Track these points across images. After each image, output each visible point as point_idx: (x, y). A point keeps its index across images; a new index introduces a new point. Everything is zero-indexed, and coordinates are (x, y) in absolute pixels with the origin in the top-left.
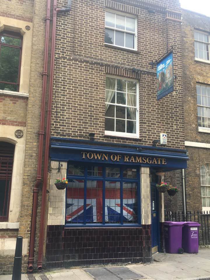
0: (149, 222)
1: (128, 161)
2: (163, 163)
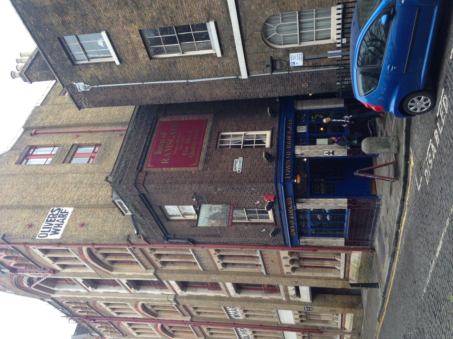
0: (346, 200)
2: (291, 199)
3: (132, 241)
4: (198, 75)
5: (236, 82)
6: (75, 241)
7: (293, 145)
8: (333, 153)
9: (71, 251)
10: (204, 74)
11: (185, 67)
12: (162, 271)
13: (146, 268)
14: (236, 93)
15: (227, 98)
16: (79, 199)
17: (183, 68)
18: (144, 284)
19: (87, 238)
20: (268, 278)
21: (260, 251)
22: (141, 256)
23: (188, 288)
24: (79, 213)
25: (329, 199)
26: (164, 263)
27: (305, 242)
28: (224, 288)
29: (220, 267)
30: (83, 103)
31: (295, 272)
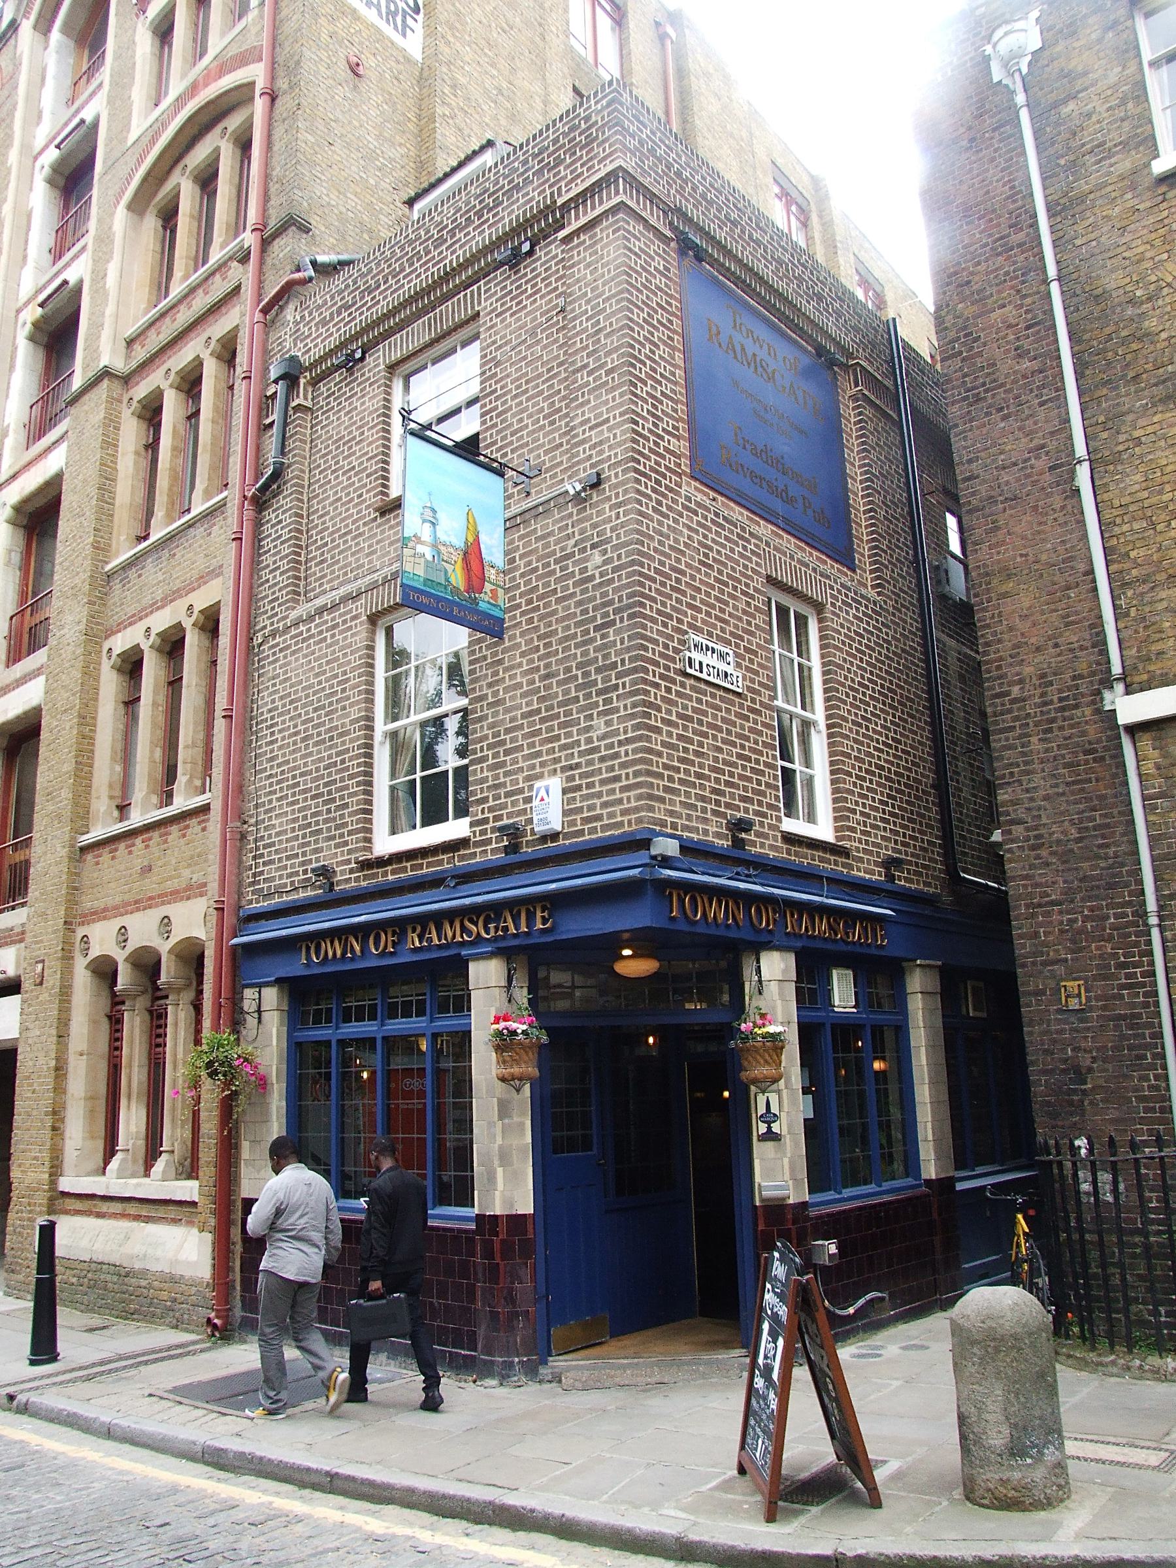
1: (417, 944)
3: (278, 243)
4: (1116, 503)
5: (1081, 677)
6: (288, 28)
7: (799, 944)
8: (770, 1136)
9: (240, 26)
10: (1125, 528)
11: (1162, 443)
12: (113, 401)
13: (130, 343)
15: (987, 644)
16: (454, 87)
17: (1153, 438)
18: (53, 364)
19: (305, 67)
20: (64, 852)
21: (205, 809)
22: (194, 307)
23: (20, 535)
24: (400, 73)
25: (528, 1123)
26: (151, 413)
27: (259, 1011)
28: (18, 675)
29: (120, 643)
31: (89, 973)
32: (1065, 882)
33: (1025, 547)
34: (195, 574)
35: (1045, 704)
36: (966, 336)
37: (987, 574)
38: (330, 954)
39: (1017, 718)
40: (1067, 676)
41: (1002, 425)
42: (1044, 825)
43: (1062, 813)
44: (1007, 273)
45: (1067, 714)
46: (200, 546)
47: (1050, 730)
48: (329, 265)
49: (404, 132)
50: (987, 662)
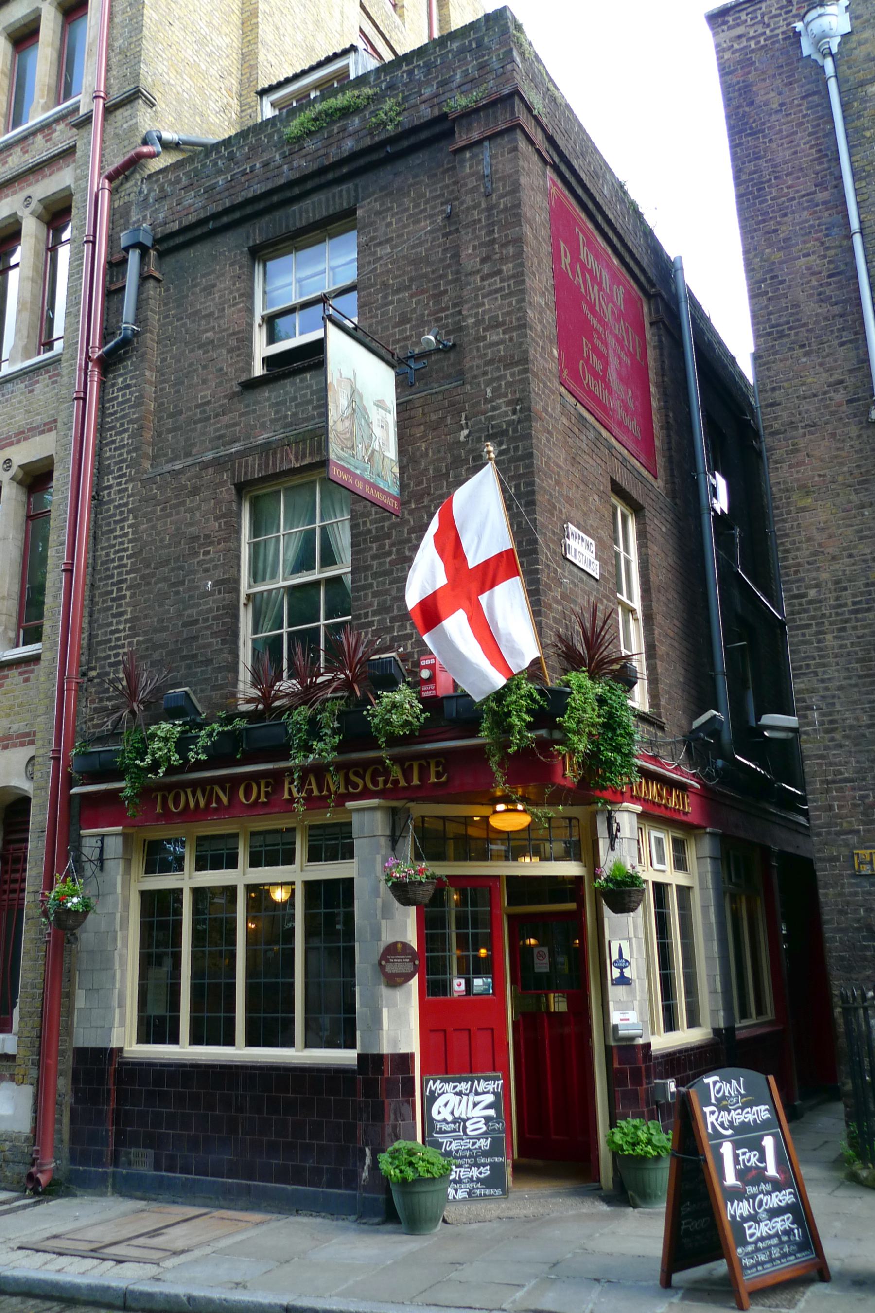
2: (433, 779)
8: (623, 981)
14: (817, 586)
15: (787, 551)
27: (101, 860)
30: (740, 30)
32: (857, 762)
33: (823, 469)
34: (14, 429)
35: (840, 606)
36: (772, 278)
37: (788, 490)
38: (192, 804)
39: (813, 618)
40: (860, 583)
41: (804, 360)
42: (838, 712)
43: (855, 702)
44: (812, 226)
45: (859, 616)
46: (20, 402)
47: (844, 629)
48: (171, 142)
49: (229, 22)
50: (786, 567)
